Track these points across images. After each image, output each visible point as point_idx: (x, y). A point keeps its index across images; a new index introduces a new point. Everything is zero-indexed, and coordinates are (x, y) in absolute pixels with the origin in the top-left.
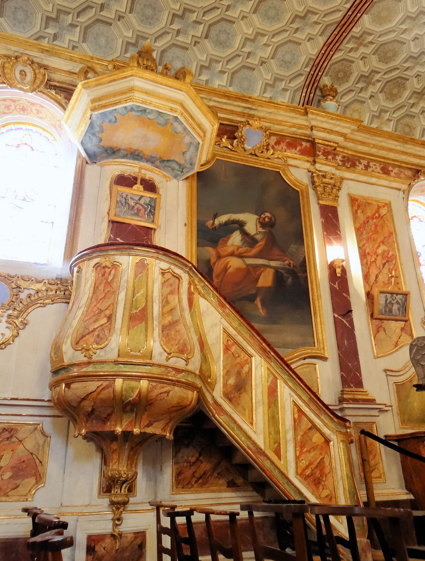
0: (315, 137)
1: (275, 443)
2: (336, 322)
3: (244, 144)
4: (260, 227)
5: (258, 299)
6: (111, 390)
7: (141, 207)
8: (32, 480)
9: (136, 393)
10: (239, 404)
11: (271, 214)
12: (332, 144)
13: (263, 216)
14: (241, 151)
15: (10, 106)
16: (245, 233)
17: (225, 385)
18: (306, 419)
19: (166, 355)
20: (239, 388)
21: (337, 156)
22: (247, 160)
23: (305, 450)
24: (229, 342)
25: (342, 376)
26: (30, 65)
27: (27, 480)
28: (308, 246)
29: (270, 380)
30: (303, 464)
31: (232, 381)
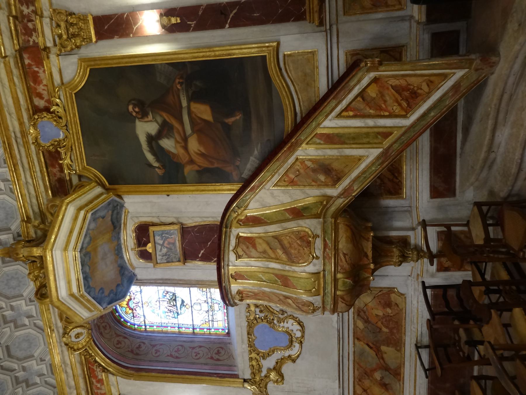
0: (14, 52)
1: (377, 137)
2: (234, 25)
3: (60, 140)
4: (148, 117)
5: (227, 121)
6: (345, 297)
7: (166, 242)
8: (393, 296)
9: (347, 280)
10: (342, 171)
11: (128, 105)
12: (12, 25)
13: (134, 114)
14: (69, 142)
15: (103, 326)
16: (160, 135)
17: (326, 185)
18: (354, 103)
19: (314, 260)
20: (330, 172)
21: (24, 13)
22: (76, 133)
23: (383, 106)
24: (286, 180)
25: (293, 21)
26: (68, 334)
27: (393, 299)
28: (155, 60)
29: (318, 141)
30: (397, 109)
31: (322, 178)
